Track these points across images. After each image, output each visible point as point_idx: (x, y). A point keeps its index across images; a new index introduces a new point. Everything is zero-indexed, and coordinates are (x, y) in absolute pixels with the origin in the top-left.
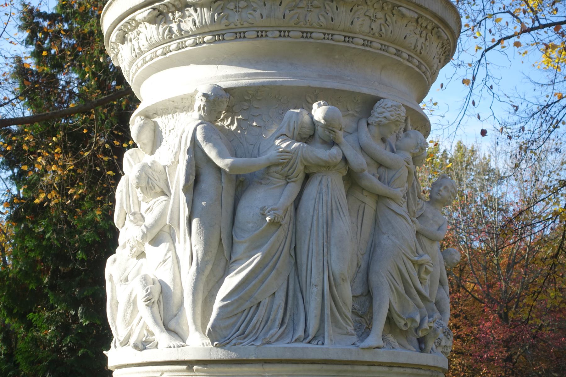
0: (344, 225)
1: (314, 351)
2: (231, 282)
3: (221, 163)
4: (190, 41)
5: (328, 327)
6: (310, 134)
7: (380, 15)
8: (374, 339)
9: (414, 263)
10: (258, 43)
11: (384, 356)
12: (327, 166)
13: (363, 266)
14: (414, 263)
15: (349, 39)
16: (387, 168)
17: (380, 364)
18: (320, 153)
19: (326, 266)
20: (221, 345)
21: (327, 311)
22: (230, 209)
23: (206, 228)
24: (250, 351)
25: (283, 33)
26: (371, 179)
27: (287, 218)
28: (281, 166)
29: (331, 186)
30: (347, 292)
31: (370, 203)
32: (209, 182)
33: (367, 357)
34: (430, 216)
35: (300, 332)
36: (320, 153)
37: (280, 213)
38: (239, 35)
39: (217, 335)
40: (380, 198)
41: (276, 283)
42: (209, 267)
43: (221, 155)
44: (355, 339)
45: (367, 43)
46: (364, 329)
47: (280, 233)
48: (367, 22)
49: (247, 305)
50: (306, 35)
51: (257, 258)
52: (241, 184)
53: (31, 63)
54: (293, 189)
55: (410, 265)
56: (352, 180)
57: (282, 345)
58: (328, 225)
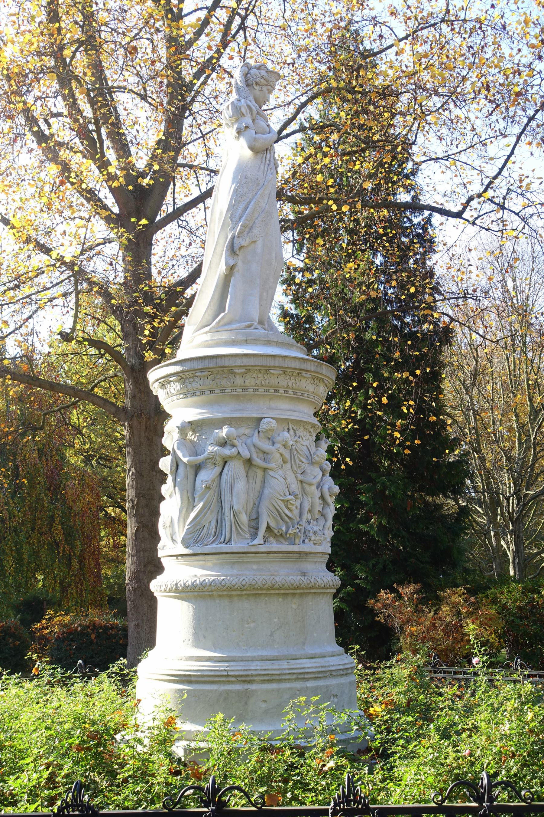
0: (240, 486)
1: (225, 548)
2: (193, 515)
3: (185, 460)
4: (175, 397)
5: (234, 537)
6: (223, 443)
7: (260, 375)
8: (259, 540)
9: (283, 501)
10: (203, 397)
11: (263, 549)
12: (232, 458)
13: (257, 503)
14: (283, 501)
15: (244, 390)
16: (268, 454)
17: (262, 553)
18: (227, 451)
19: (232, 507)
20: (187, 547)
21: (234, 529)
22: (192, 481)
23: (181, 491)
24: (198, 550)
25: (212, 392)
26: (258, 461)
27: (215, 484)
28: (211, 458)
29: (235, 468)
30: (244, 518)
31: (260, 473)
32: (181, 468)
33: (253, 550)
34: (309, 471)
35: (222, 540)
36: (227, 451)
37: (209, 482)
38: (193, 395)
39: (186, 542)
40: (265, 470)
41: (211, 517)
42: (185, 510)
43: (184, 456)
44: (249, 541)
45: (255, 390)
46: (254, 536)
47: (211, 492)
48: (253, 380)
49: (198, 527)
50: (223, 391)
51: (201, 504)
52: (197, 468)
53: (291, 309)
54: (218, 470)
55: (280, 503)
56: (249, 462)
57: (213, 545)
58: (232, 487)
